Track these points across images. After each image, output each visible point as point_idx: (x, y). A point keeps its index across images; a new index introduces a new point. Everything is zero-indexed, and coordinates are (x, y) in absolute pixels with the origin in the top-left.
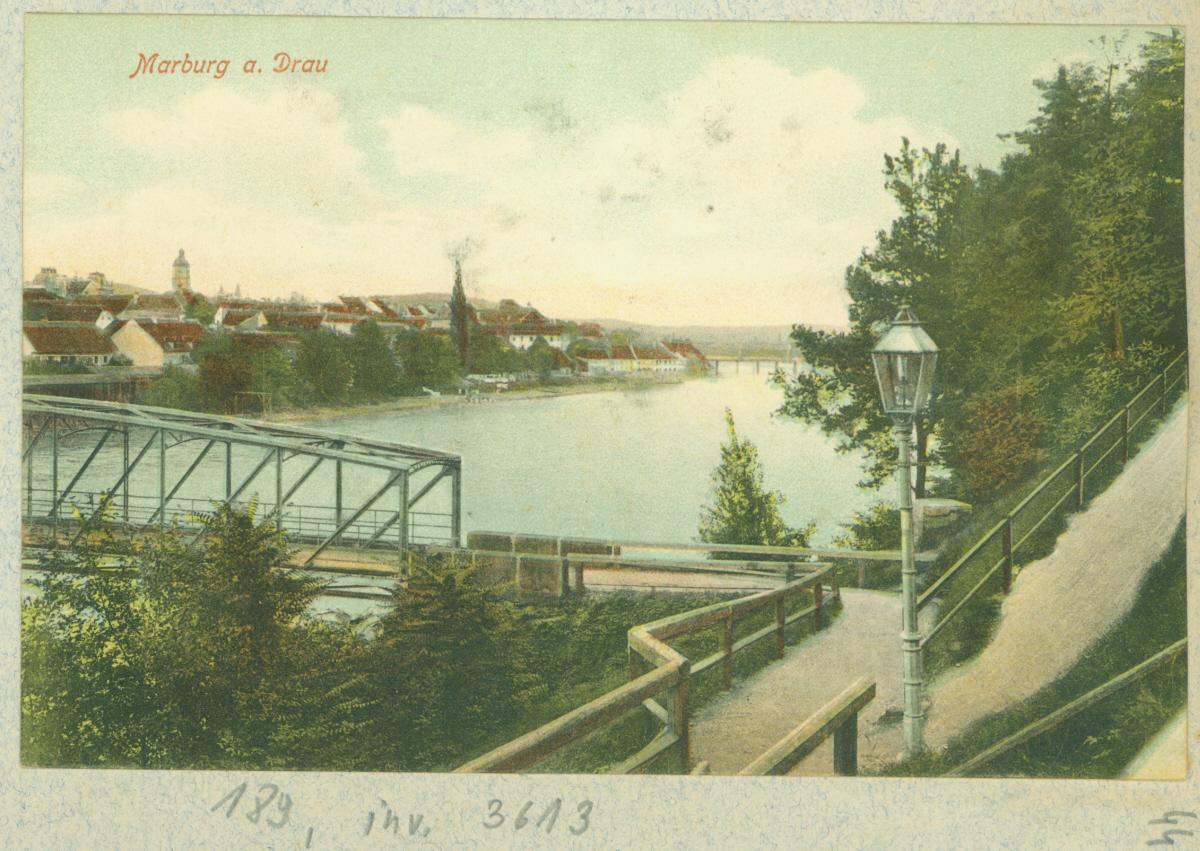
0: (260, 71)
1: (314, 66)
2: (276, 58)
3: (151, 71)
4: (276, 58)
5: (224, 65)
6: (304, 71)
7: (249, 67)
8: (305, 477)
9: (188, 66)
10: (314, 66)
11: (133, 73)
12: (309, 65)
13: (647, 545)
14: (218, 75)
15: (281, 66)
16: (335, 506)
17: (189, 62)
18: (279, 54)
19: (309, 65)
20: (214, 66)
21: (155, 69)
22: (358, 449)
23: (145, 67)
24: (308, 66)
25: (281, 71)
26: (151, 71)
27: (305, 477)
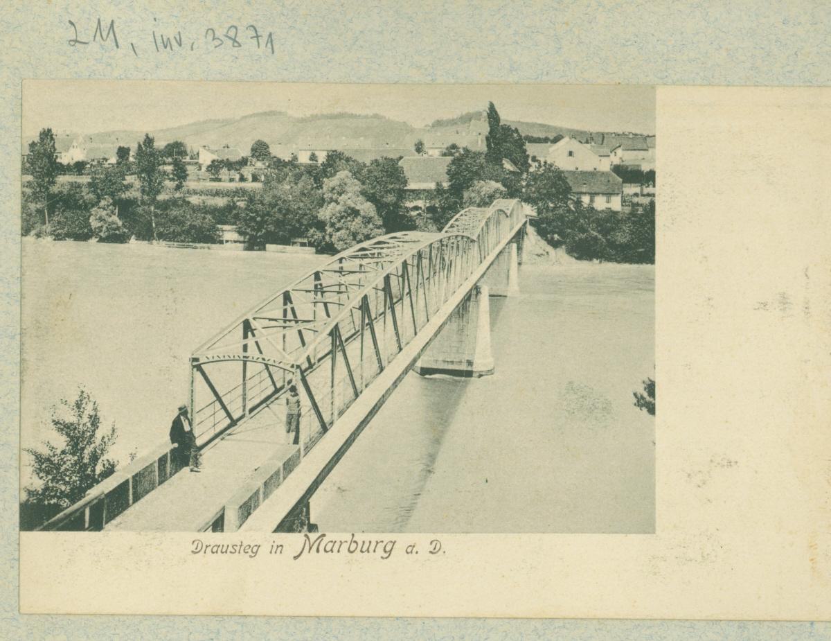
0: (417, 553)
1: (220, 549)
2: (431, 543)
3: (318, 551)
4: (431, 543)
5: (352, 549)
6: (213, 553)
7: (409, 550)
8: (413, 317)
9: (353, 547)
10: (220, 549)
11: (296, 554)
12: (410, 548)
13: (399, 284)
14: (253, 555)
15: (435, 549)
16: (226, 415)
17: (356, 542)
18: (434, 541)
19: (410, 548)
20: (381, 546)
21: (321, 548)
22: (452, 275)
23: (310, 548)
24: (215, 549)
25: (197, 553)
26: (318, 551)
27: (413, 317)
